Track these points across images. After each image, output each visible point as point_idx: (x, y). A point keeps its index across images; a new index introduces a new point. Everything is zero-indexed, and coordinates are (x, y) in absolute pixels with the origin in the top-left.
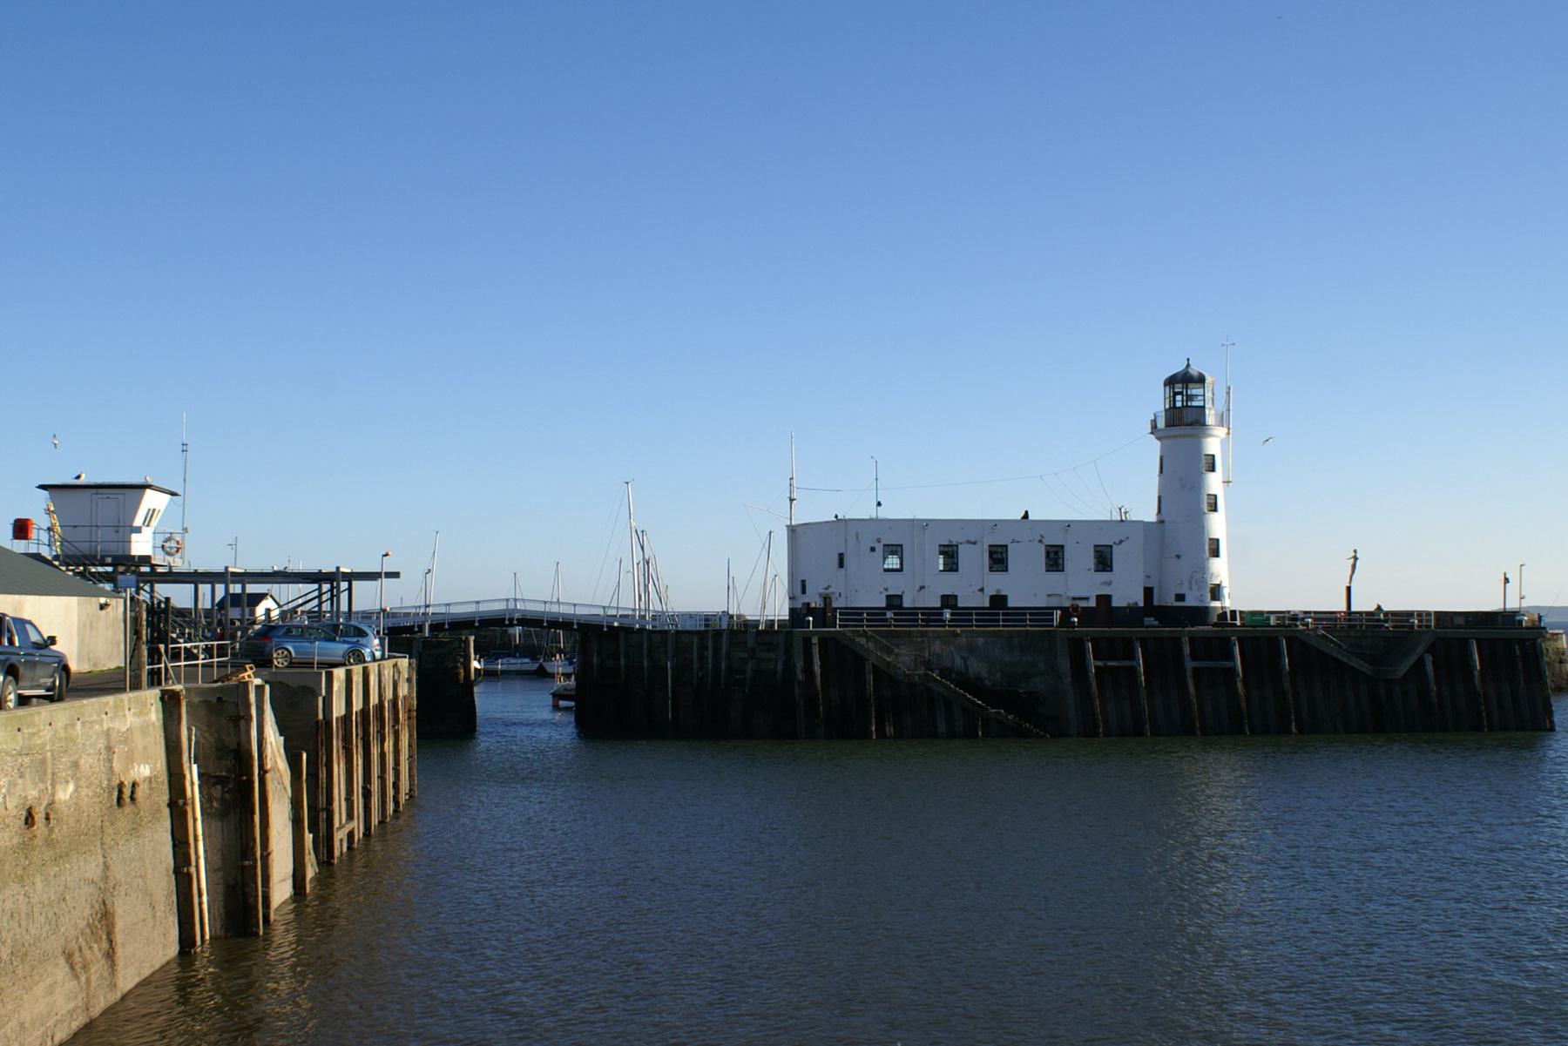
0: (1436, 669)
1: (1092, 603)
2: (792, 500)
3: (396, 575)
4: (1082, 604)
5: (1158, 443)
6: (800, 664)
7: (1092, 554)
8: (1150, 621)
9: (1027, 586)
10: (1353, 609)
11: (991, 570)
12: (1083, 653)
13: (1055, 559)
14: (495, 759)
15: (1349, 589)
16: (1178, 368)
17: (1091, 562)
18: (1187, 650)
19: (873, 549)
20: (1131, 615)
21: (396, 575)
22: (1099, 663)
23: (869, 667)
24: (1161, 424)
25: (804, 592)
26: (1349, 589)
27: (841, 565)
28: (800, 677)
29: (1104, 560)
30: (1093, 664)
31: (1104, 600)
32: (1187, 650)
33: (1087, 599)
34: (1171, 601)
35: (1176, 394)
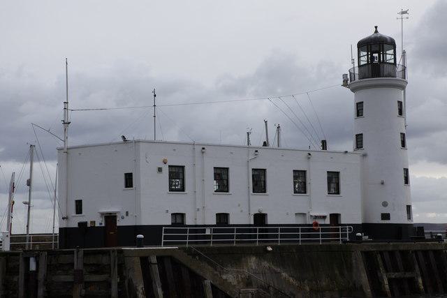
4: (320, 222)
7: (124, 175)
9: (282, 208)
16: (368, 33)
19: (160, 170)
27: (401, 112)
33: (324, 217)
34: (377, 220)
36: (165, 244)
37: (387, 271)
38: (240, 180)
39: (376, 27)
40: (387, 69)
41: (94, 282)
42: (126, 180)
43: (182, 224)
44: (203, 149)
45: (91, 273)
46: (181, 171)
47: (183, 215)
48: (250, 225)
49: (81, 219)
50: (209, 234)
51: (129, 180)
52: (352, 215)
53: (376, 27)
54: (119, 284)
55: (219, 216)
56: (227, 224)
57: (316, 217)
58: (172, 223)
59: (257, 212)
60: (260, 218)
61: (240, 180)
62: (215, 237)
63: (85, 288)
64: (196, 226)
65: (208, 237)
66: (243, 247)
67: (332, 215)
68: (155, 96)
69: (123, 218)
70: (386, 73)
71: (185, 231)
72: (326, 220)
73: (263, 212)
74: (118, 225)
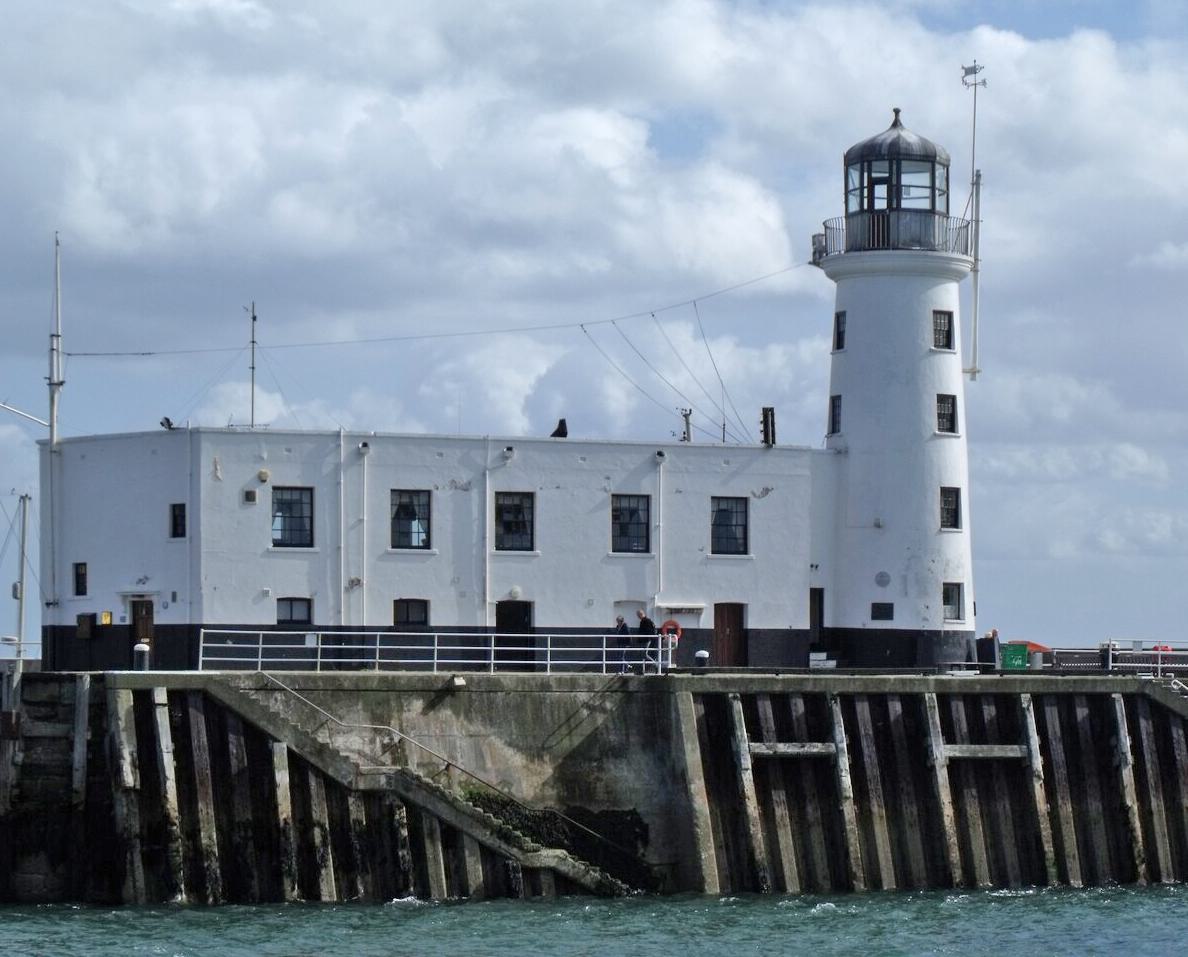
1: (707, 622)
2: (54, 385)
3: (768, 415)
5: (832, 285)
8: (818, 659)
9: (575, 586)
10: (828, 622)
13: (631, 526)
16: (872, 128)
17: (760, 522)
18: (935, 718)
19: (249, 497)
21: (768, 415)
22: (761, 748)
24: (840, 244)
25: (81, 588)
30: (747, 749)
32: (935, 718)
33: (695, 612)
35: (873, 183)
37: (756, 735)
38: (680, 521)
39: (897, 112)
40: (904, 228)
41: (45, 738)
43: (307, 624)
44: (510, 449)
46: (642, 506)
47: (424, 605)
49: (84, 606)
50: (314, 646)
51: (178, 522)
52: (778, 610)
53: (897, 112)
54: (89, 744)
55: (287, 602)
56: (423, 624)
58: (279, 622)
61: (680, 521)
62: (326, 653)
63: (26, 750)
65: (313, 652)
66: (156, 670)
67: (719, 609)
68: (254, 318)
69: (166, 607)
70: (904, 236)
72: (703, 616)
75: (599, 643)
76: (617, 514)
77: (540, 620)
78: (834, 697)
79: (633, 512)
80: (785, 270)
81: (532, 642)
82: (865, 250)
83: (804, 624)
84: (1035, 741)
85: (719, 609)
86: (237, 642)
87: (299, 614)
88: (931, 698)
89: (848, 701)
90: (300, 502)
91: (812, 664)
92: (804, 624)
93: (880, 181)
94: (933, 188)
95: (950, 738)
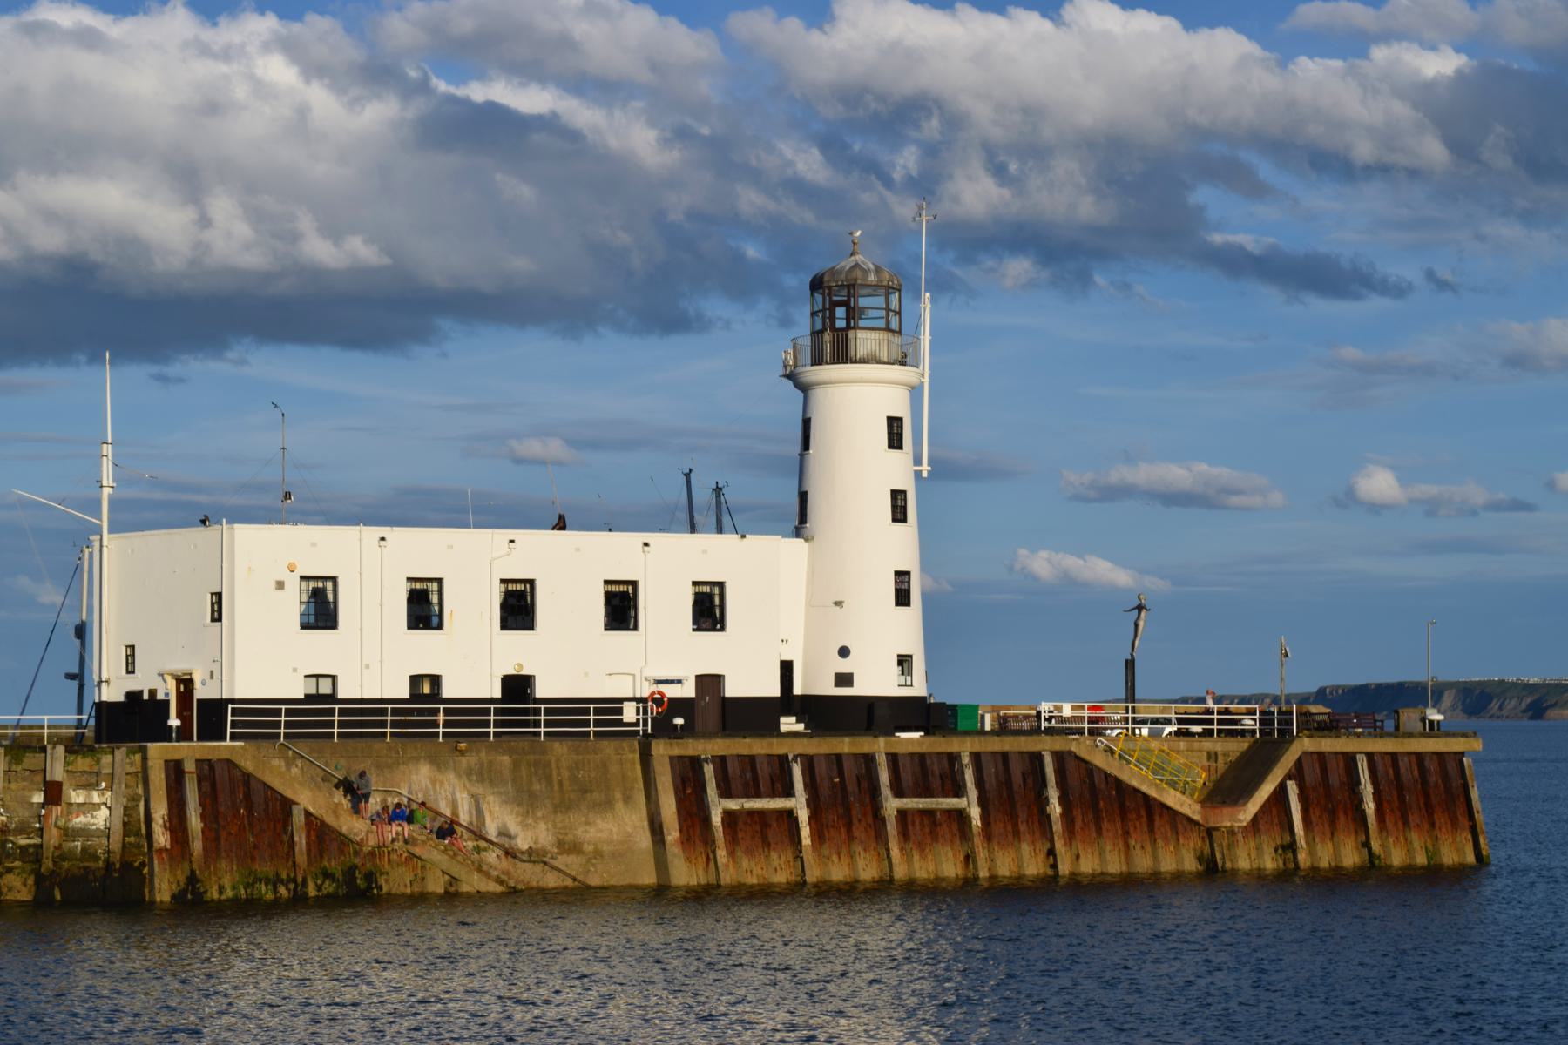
0: (1377, 796)
4: (671, 692)
6: (160, 812)
8: (788, 723)
11: (504, 627)
12: (701, 787)
14: (169, 978)
15: (1130, 665)
17: (597, 610)
18: (884, 777)
19: (280, 585)
20: (753, 716)
23: (298, 819)
26: (1130, 665)
28: (162, 838)
29: (708, 610)
31: (710, 683)
32: (884, 777)
34: (828, 689)
36: (234, 737)
42: (894, 507)
43: (435, 697)
45: (79, 787)
46: (716, 590)
47: (435, 680)
48: (492, 701)
49: (133, 684)
55: (416, 680)
57: (659, 682)
59: (512, 672)
60: (517, 687)
64: (362, 701)
70: (862, 352)
71: (537, 712)
73: (524, 672)
74: (693, 694)
75: (587, 711)
76: (609, 597)
77: (541, 691)
78: (706, 760)
79: (522, 594)
80: (825, 383)
81: (525, 712)
82: (879, 362)
83: (775, 691)
84: (973, 793)
85: (701, 680)
86: (259, 713)
87: (325, 688)
88: (882, 760)
89: (809, 763)
90: (324, 589)
91: (783, 728)
92: (775, 691)
93: (840, 304)
94: (888, 309)
95: (899, 792)
